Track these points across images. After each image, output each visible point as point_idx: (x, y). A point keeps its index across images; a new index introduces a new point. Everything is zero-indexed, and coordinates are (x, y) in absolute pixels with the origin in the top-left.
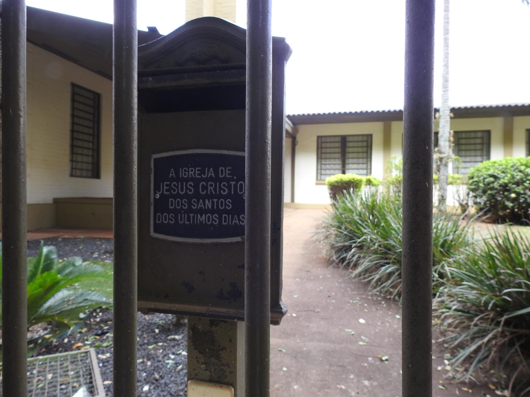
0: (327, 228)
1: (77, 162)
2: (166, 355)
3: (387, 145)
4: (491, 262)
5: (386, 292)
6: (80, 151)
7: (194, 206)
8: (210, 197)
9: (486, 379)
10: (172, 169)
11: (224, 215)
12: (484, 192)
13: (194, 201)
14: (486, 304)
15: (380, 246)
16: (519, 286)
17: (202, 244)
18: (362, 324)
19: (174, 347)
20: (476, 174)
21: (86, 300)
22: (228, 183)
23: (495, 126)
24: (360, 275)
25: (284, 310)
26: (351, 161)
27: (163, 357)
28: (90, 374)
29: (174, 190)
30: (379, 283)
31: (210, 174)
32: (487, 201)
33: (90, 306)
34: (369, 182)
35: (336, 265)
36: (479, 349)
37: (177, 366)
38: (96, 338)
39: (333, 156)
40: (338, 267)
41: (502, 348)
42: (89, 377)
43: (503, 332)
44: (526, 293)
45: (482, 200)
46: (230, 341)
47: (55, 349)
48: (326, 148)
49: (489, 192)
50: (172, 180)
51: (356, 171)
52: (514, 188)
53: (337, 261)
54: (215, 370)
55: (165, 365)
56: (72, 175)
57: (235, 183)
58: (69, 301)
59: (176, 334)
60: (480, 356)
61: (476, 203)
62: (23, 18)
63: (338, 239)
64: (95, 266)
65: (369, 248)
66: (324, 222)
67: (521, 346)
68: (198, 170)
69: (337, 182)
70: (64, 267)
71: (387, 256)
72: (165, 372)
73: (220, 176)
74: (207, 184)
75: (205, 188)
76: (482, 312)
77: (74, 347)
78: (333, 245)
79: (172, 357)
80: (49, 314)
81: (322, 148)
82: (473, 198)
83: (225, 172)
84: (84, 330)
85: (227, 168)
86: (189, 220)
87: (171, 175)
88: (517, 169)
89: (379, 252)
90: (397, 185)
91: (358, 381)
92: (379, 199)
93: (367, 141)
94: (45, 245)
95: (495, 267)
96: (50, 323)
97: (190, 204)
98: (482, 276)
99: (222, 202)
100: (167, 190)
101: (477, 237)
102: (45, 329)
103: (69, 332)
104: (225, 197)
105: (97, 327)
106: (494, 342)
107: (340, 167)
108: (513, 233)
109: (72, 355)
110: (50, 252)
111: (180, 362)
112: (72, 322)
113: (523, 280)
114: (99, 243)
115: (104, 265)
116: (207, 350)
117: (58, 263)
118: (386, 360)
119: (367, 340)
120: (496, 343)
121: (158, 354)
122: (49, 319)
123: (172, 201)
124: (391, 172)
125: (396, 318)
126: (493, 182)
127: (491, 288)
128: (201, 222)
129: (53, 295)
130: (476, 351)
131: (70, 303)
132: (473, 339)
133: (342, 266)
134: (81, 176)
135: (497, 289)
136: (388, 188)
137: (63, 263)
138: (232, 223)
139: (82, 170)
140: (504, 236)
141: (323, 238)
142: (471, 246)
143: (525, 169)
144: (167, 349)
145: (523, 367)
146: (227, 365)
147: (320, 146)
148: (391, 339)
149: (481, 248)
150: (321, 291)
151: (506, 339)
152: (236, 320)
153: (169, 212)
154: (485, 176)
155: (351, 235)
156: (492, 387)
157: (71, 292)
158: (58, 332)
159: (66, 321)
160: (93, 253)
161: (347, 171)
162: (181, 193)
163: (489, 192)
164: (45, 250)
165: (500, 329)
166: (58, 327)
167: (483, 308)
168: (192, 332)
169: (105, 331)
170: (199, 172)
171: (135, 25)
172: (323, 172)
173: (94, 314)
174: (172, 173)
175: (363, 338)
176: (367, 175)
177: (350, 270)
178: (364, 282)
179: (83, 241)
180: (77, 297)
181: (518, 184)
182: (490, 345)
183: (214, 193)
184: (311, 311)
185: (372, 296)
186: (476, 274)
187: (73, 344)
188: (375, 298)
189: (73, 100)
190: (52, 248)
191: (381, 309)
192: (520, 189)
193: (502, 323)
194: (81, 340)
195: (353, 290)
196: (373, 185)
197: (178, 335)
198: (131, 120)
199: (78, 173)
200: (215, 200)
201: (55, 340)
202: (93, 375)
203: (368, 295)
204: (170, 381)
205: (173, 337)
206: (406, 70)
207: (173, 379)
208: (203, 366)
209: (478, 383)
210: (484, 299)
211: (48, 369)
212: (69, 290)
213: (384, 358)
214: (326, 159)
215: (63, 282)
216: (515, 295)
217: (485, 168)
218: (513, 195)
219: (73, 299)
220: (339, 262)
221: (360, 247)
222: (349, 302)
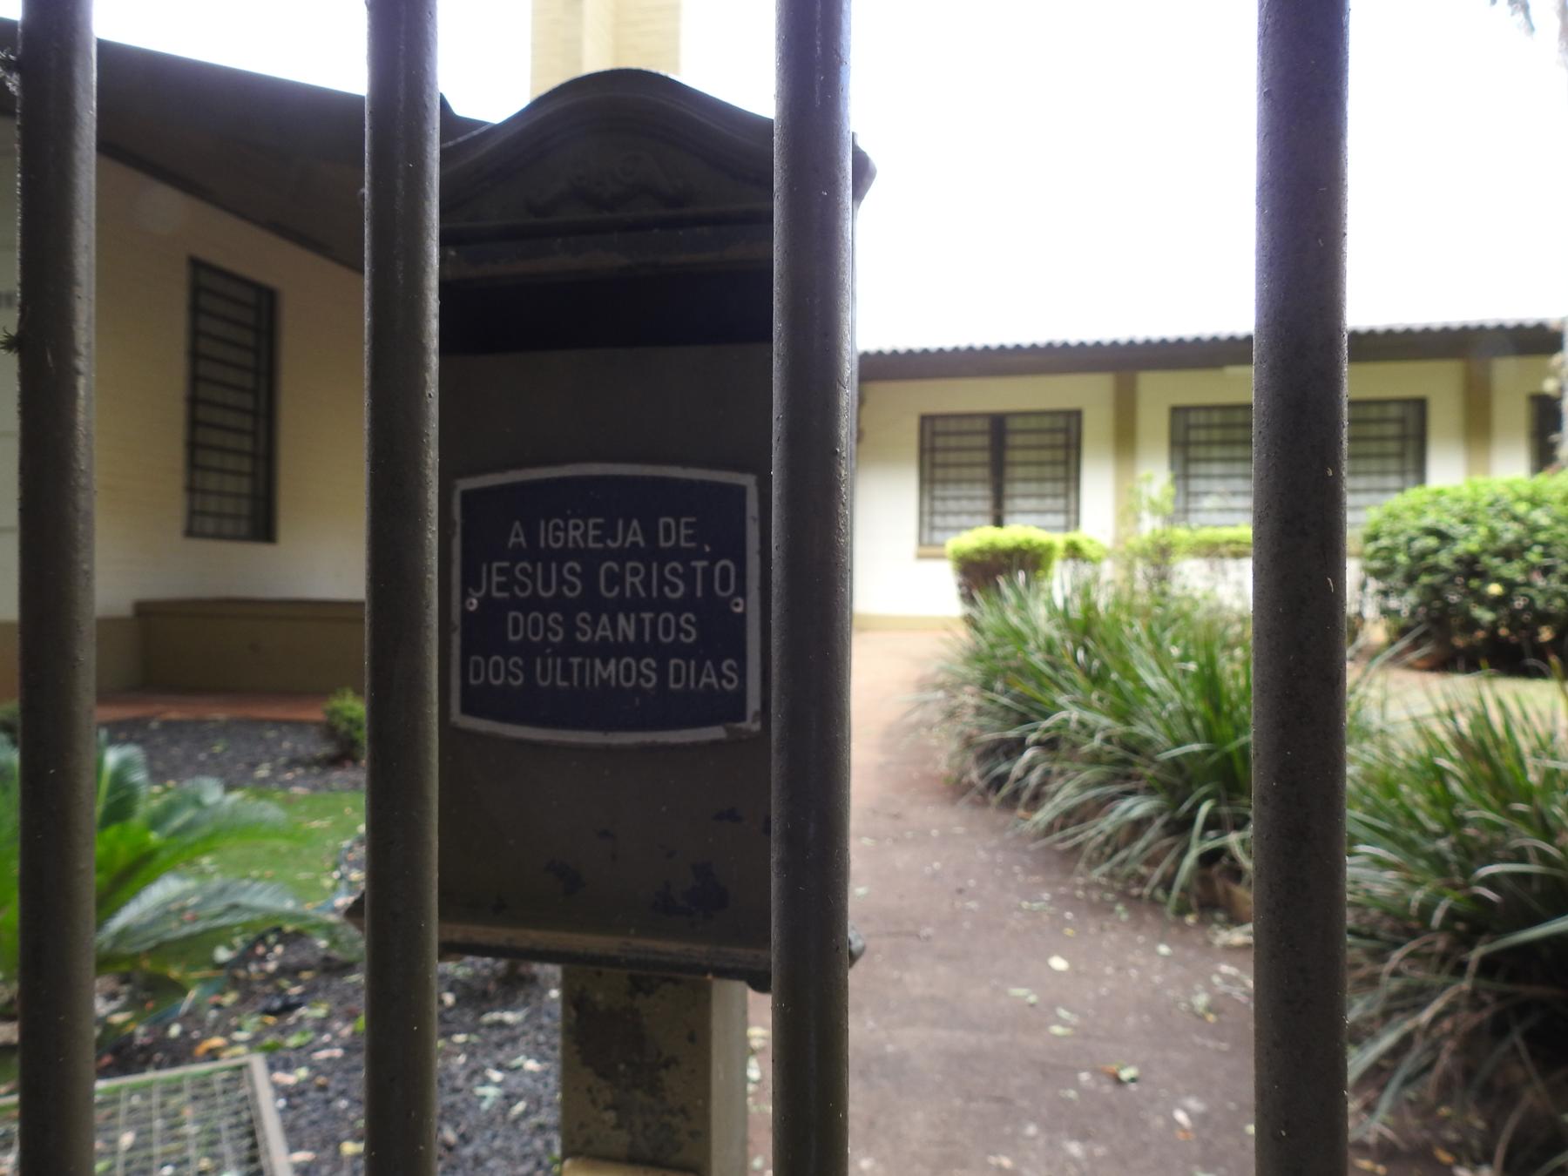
0: (951, 688)
1: (205, 492)
2: (477, 1074)
3: (1125, 441)
4: (1436, 787)
5: (1129, 877)
6: (214, 460)
7: (584, 634)
8: (631, 606)
9: (1426, 1135)
10: (517, 524)
11: (673, 662)
12: (1411, 579)
13: (584, 620)
14: (1426, 910)
15: (1108, 740)
16: (1520, 856)
17: (608, 749)
18: (1058, 974)
19: (500, 1046)
20: (1386, 527)
21: (234, 907)
22: (686, 563)
23: (1438, 384)
24: (1050, 829)
25: (856, 944)
26: (1019, 488)
27: (470, 1078)
28: (252, 1133)
29: (523, 587)
30: (1108, 850)
31: (630, 539)
32: (1421, 604)
33: (246, 927)
34: (1074, 551)
35: (979, 798)
36: (1406, 1042)
37: (511, 1106)
38: (265, 1024)
39: (966, 472)
40: (985, 803)
41: (1470, 1043)
42: (247, 1142)
43: (1474, 994)
44: (1542, 877)
45: (1405, 603)
46: (692, 1038)
47: (141, 1057)
48: (947, 449)
49: (1425, 579)
50: (517, 555)
51: (1034, 518)
52: (1497, 567)
53: (982, 784)
54: (646, 1126)
55: (474, 1103)
56: (190, 533)
57: (704, 563)
58: (183, 910)
59: (506, 1006)
60: (1408, 1065)
61: (1386, 612)
62: (87, 68)
63: (984, 720)
64: (262, 803)
65: (1075, 746)
66: (942, 670)
67: (1529, 1036)
68: (596, 526)
69: (980, 551)
70: (170, 809)
71: (1130, 770)
72: (473, 1123)
73: (662, 544)
74: (622, 566)
75: (615, 579)
76: (1412, 934)
77: (201, 1050)
78: (970, 737)
79: (496, 1076)
80: (125, 949)
81: (933, 450)
82: (1379, 598)
83: (676, 532)
84: (230, 998)
85: (683, 520)
86: (567, 671)
87: (513, 540)
88: (1504, 510)
89: (1105, 758)
90: (1157, 559)
91: (1050, 1143)
92: (1102, 600)
93: (1066, 431)
94: (113, 741)
95: (1450, 801)
96: (125, 979)
97: (571, 629)
98: (1411, 827)
99: (667, 621)
100: (501, 587)
101: (1396, 712)
102: (112, 996)
103: (185, 1005)
104: (678, 608)
105: (269, 989)
106: (1447, 1024)
107: (986, 505)
108: (1501, 704)
109: (194, 1077)
110: (125, 765)
111: (520, 1090)
112: (195, 975)
113: (1530, 841)
114: (271, 734)
115: (289, 802)
116: (622, 1067)
117: (151, 796)
118: (1133, 1080)
119: (1074, 1020)
120: (1455, 1026)
121: (454, 1069)
122: (125, 968)
123: (516, 620)
124: (1138, 520)
125: (1157, 953)
126: (1435, 551)
127: (1438, 863)
128: (605, 683)
129: (135, 894)
130: (1396, 1052)
131: (188, 915)
132: (1386, 1016)
133: (994, 799)
134: (218, 536)
135: (1454, 867)
136: (1130, 567)
137: (167, 797)
138: (697, 682)
139: (219, 515)
140: (1474, 710)
141: (938, 717)
142: (1378, 738)
143: (1528, 512)
144: (479, 1055)
145: (1533, 1096)
146: (683, 1110)
147: (927, 445)
148: (1146, 1018)
149: (1406, 744)
150: (935, 876)
151: (1486, 1014)
152: (710, 977)
153: (507, 650)
154: (1413, 532)
155: (1022, 708)
156: (1445, 1157)
157: (191, 884)
158: (150, 1005)
159: (174, 973)
160: (253, 766)
161: (1007, 519)
162: (543, 594)
163: (1425, 579)
164: (112, 757)
165: (1466, 985)
166: (152, 990)
167: (1415, 924)
168: (574, 1014)
169: (293, 1000)
170: (598, 532)
171: (87, 24)
172: (938, 521)
173: (260, 950)
174: (517, 535)
175: (1063, 1013)
176: (1066, 528)
177: (1021, 812)
178: (1062, 850)
179: (224, 730)
180: (207, 900)
181: (1508, 554)
182: (1435, 1033)
183: (643, 594)
184: (909, 934)
185: (1087, 887)
186: (1395, 822)
187: (197, 1042)
188: (1095, 896)
189: (195, 310)
190: (132, 751)
191: (1114, 929)
192: (1513, 571)
193: (1472, 967)
194: (221, 1029)
195: (1029, 872)
196: (1085, 559)
197: (514, 1010)
198: (419, 386)
199: (210, 525)
200: (647, 616)
201: (140, 1030)
202: (259, 1136)
203: (1076, 887)
204: (490, 1148)
205: (495, 1016)
206: (1259, 241)
207: (498, 1143)
208: (610, 1116)
209: (1402, 1146)
210: (1418, 896)
211: (121, 1119)
212: (183, 877)
213: (1126, 1074)
214: (945, 481)
215: (163, 856)
216: (1508, 884)
217: (1413, 508)
218: (1495, 589)
219: (197, 906)
220: (989, 787)
221: (1050, 744)
222: (1019, 909)
